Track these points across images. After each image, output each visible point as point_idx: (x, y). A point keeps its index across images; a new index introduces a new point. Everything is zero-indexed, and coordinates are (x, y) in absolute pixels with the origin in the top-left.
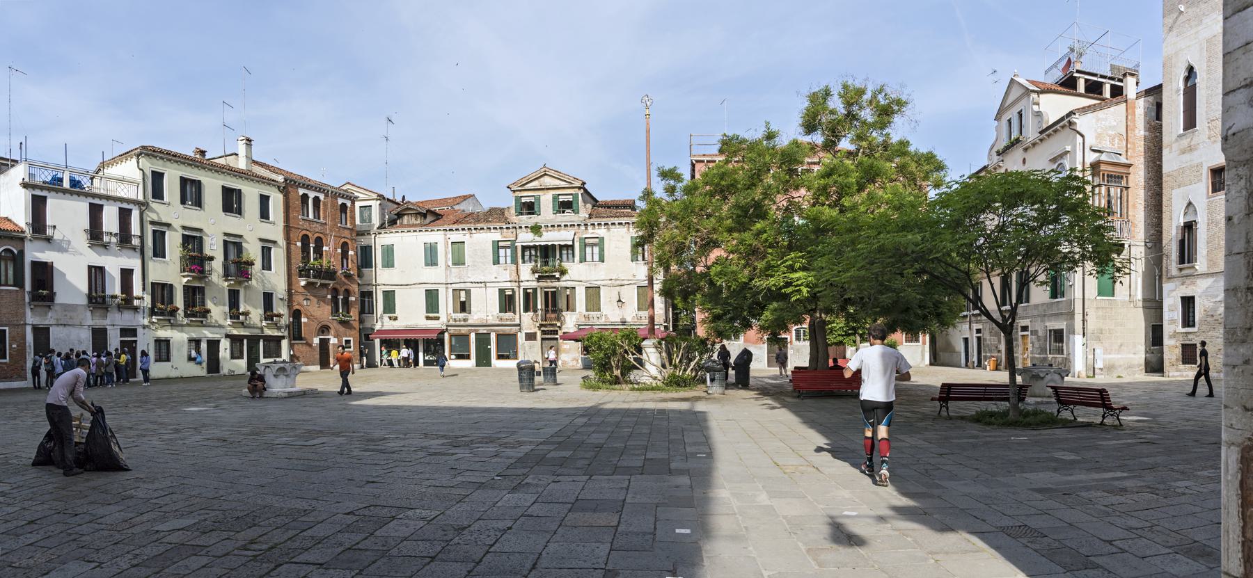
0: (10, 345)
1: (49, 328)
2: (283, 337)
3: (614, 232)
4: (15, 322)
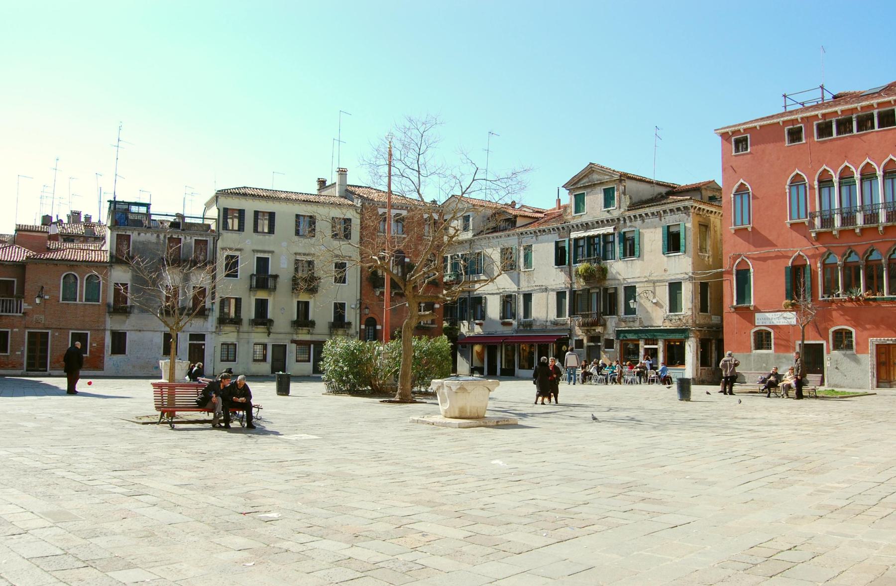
0: (91, 344)
3: (648, 223)
4: (96, 328)
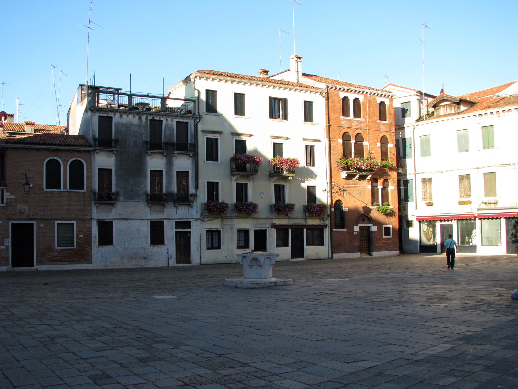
0: (78, 235)
1: (112, 222)
2: (326, 226)
4: (83, 217)
